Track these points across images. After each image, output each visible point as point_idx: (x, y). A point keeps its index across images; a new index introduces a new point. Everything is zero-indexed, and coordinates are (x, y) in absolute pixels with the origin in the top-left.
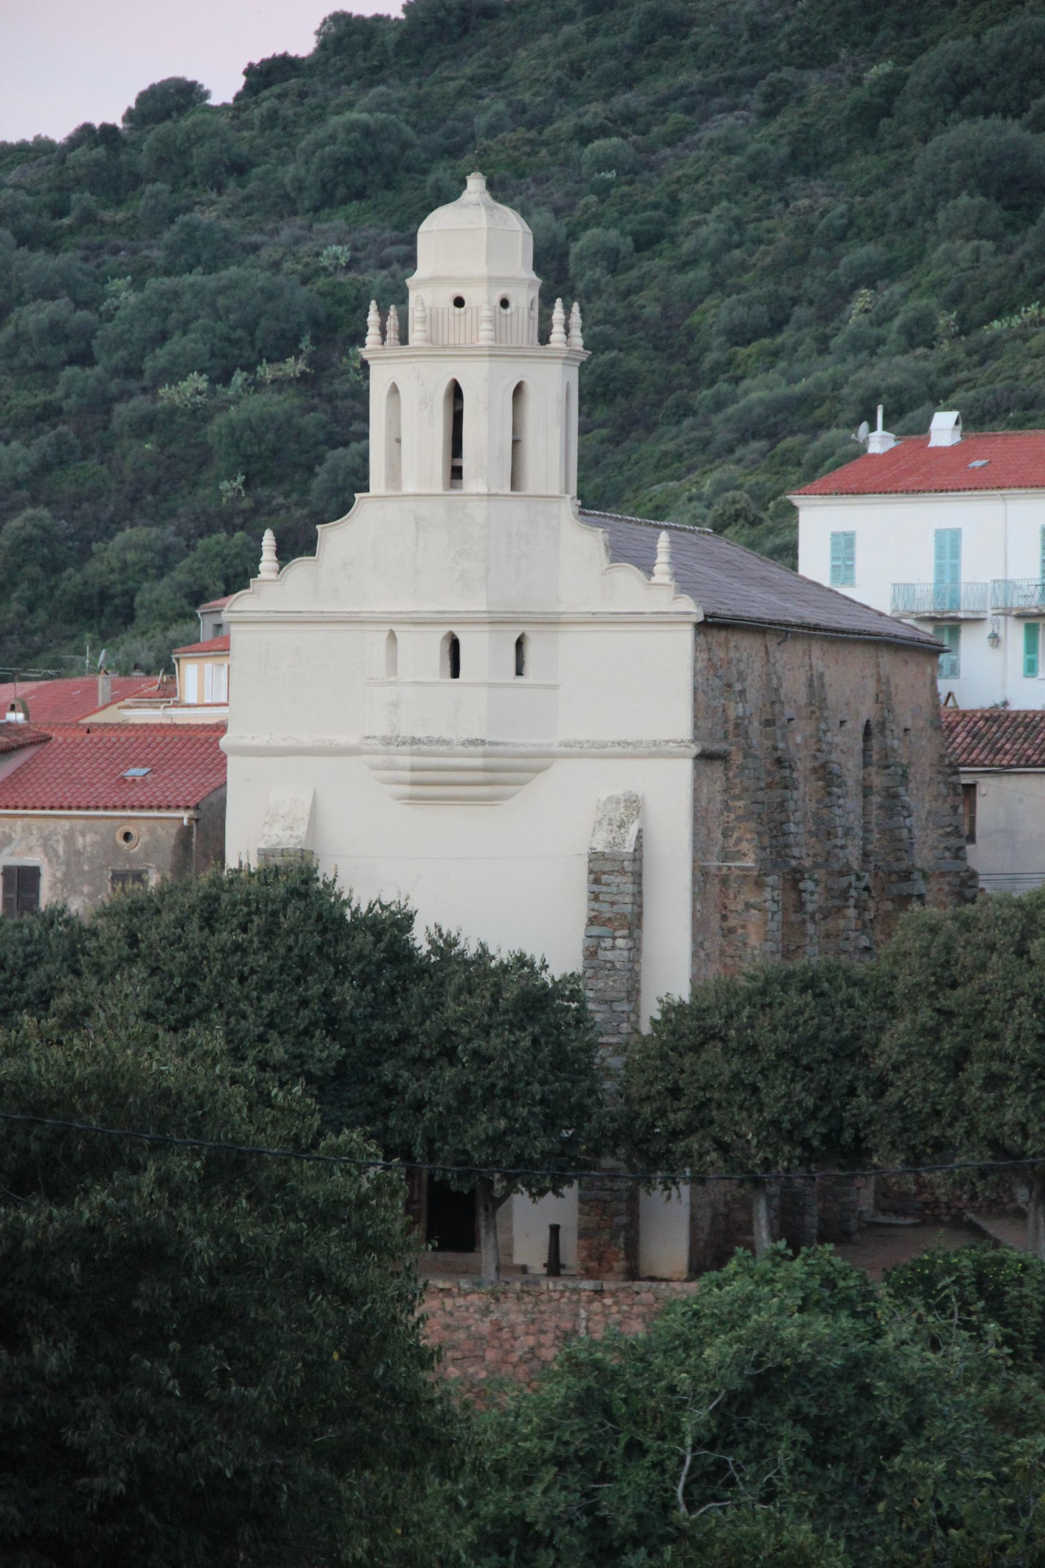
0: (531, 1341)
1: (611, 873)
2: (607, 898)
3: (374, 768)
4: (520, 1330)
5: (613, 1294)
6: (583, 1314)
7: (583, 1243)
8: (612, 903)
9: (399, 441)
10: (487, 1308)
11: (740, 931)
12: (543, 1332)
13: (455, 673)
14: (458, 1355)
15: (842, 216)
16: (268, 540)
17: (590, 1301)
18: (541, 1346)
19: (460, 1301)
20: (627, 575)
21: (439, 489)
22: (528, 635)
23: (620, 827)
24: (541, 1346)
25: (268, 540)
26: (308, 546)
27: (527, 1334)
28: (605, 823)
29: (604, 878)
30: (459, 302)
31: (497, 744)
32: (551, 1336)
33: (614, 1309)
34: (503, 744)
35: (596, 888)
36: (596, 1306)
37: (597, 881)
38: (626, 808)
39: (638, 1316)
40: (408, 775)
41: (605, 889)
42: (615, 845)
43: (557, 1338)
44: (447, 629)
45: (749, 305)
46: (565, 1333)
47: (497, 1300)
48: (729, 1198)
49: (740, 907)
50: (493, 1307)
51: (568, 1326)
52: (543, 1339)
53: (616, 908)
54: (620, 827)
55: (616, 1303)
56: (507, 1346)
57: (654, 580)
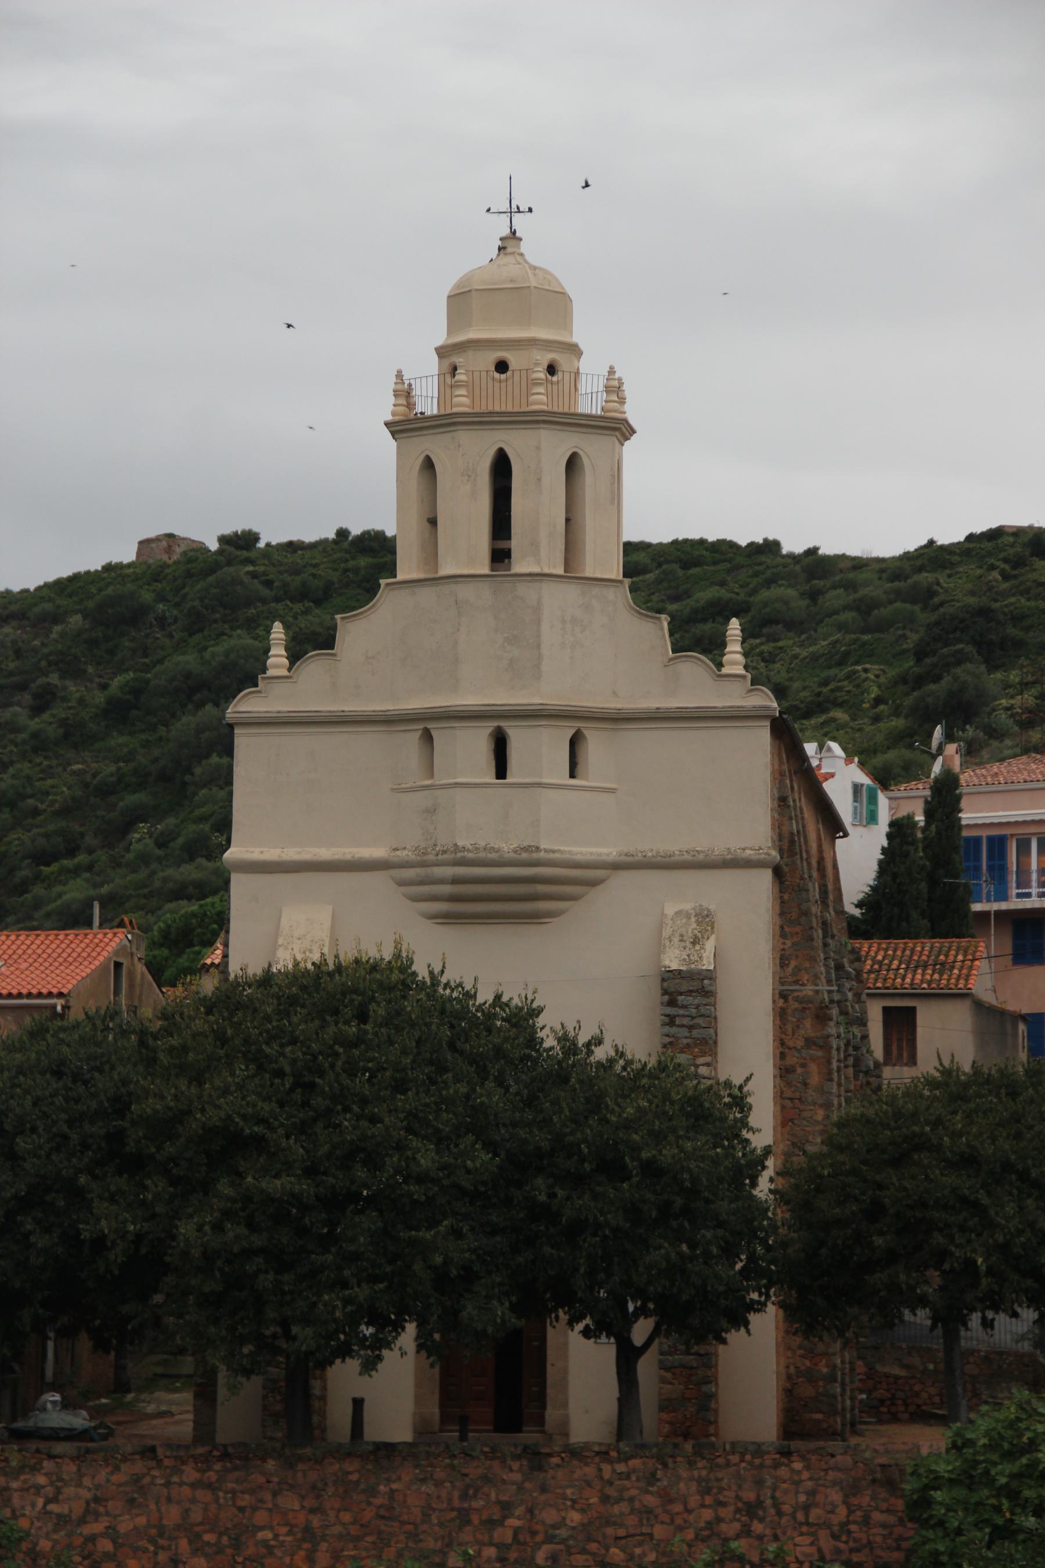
0: (707, 1514)
1: (690, 992)
2: (686, 1021)
3: (401, 883)
4: (694, 1501)
5: (803, 1458)
6: (769, 1482)
7: (664, 1416)
8: (691, 1028)
9: (433, 522)
10: (653, 1475)
11: (799, 1070)
12: (722, 1504)
13: (501, 771)
14: (621, 1532)
15: (112, 775)
16: (278, 631)
17: (776, 1466)
18: (719, 1520)
19: (621, 1468)
20: (694, 669)
21: (486, 570)
22: (586, 732)
23: (694, 943)
24: (719, 1520)
25: (278, 631)
26: (326, 641)
27: (703, 1506)
28: (676, 940)
29: (680, 998)
30: (502, 367)
31: (554, 851)
32: (732, 1508)
33: (805, 1475)
34: (559, 851)
35: (670, 1010)
36: (783, 1472)
37: (672, 1003)
38: (698, 923)
39: (834, 1483)
40: (446, 889)
41: (681, 1012)
42: (691, 962)
43: (738, 1510)
44: (496, 724)
45: (47, 836)
46: (748, 1504)
47: (665, 1465)
48: (792, 1370)
49: (800, 1043)
50: (659, 1474)
51: (750, 1495)
52: (723, 1512)
53: (695, 1032)
54: (694, 943)
55: (808, 1467)
56: (679, 1521)
57: (725, 670)
